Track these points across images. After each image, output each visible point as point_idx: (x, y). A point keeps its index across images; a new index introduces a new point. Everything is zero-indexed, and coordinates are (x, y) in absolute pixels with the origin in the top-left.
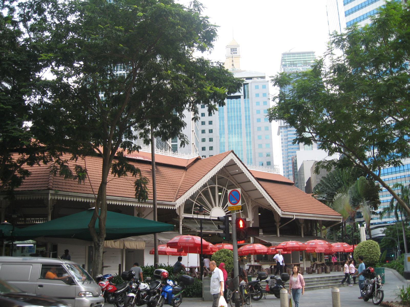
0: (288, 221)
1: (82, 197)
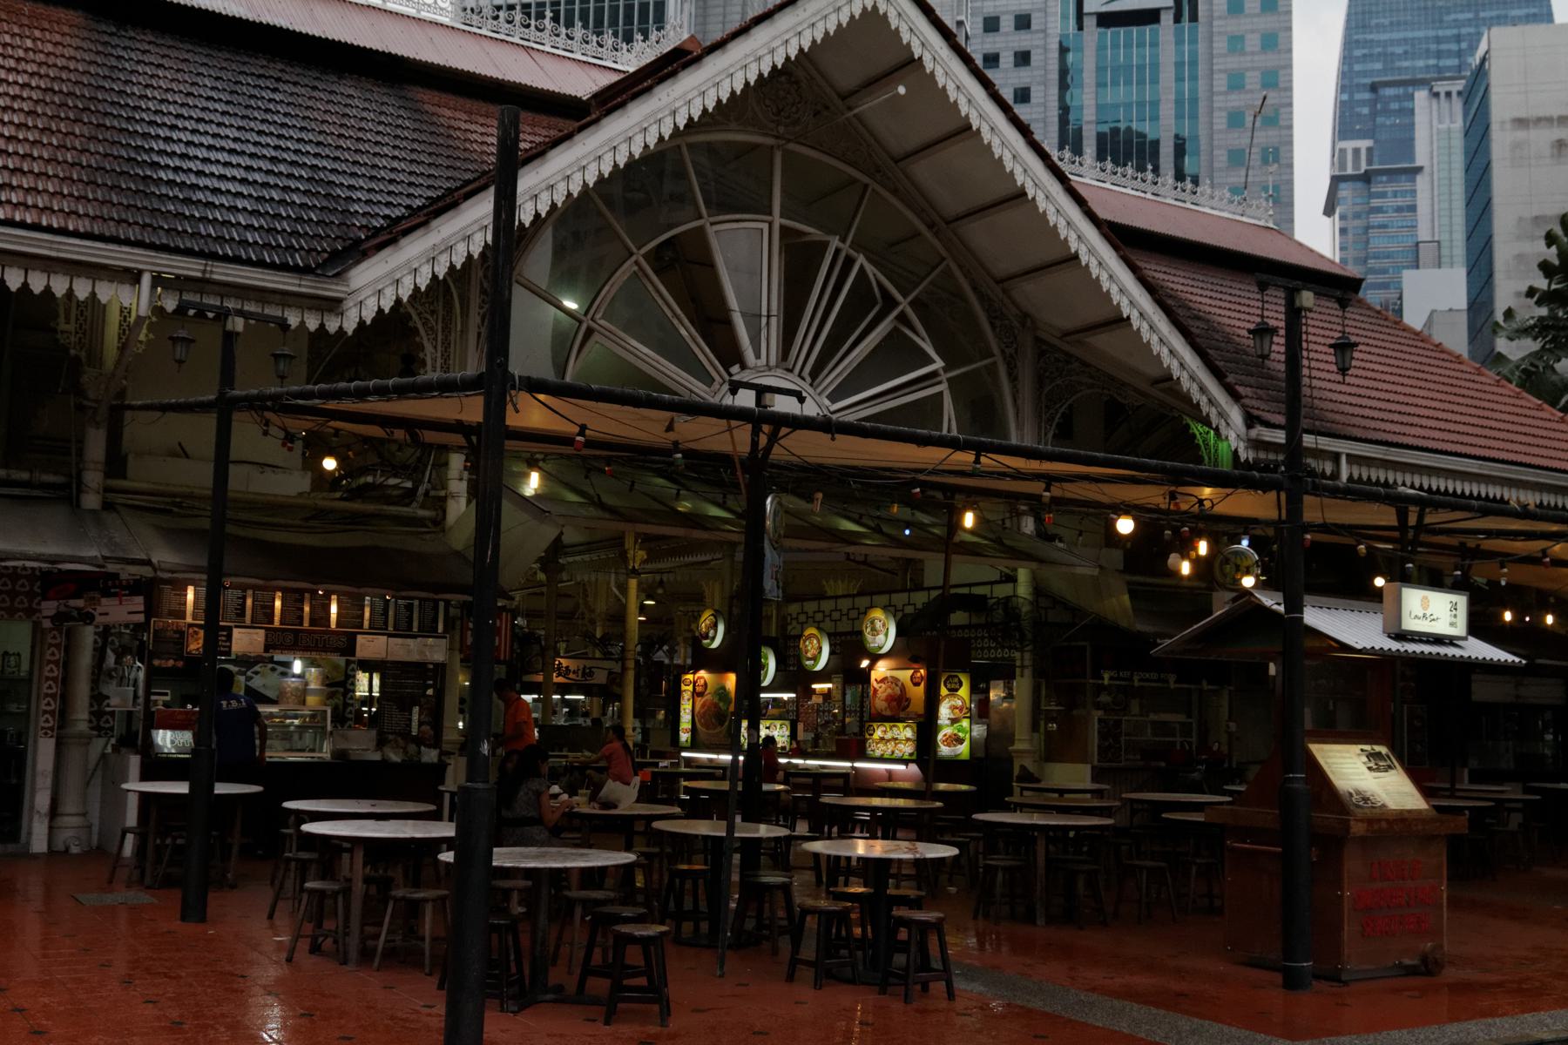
0: (964, 374)
1: (50, 264)
